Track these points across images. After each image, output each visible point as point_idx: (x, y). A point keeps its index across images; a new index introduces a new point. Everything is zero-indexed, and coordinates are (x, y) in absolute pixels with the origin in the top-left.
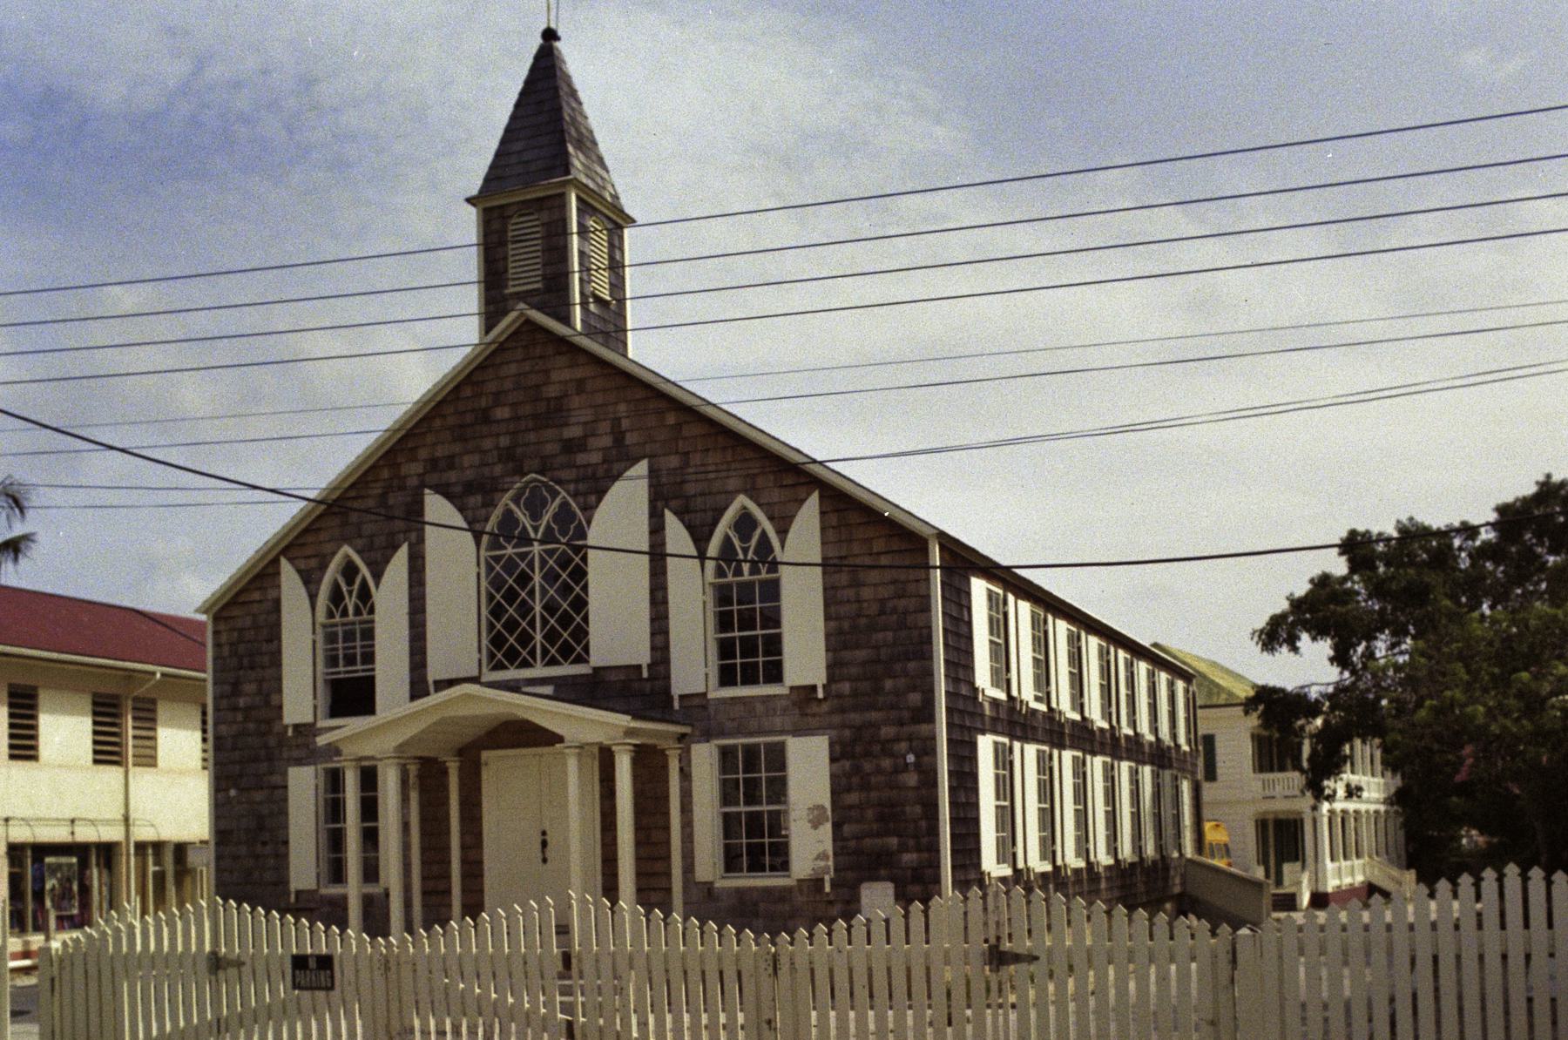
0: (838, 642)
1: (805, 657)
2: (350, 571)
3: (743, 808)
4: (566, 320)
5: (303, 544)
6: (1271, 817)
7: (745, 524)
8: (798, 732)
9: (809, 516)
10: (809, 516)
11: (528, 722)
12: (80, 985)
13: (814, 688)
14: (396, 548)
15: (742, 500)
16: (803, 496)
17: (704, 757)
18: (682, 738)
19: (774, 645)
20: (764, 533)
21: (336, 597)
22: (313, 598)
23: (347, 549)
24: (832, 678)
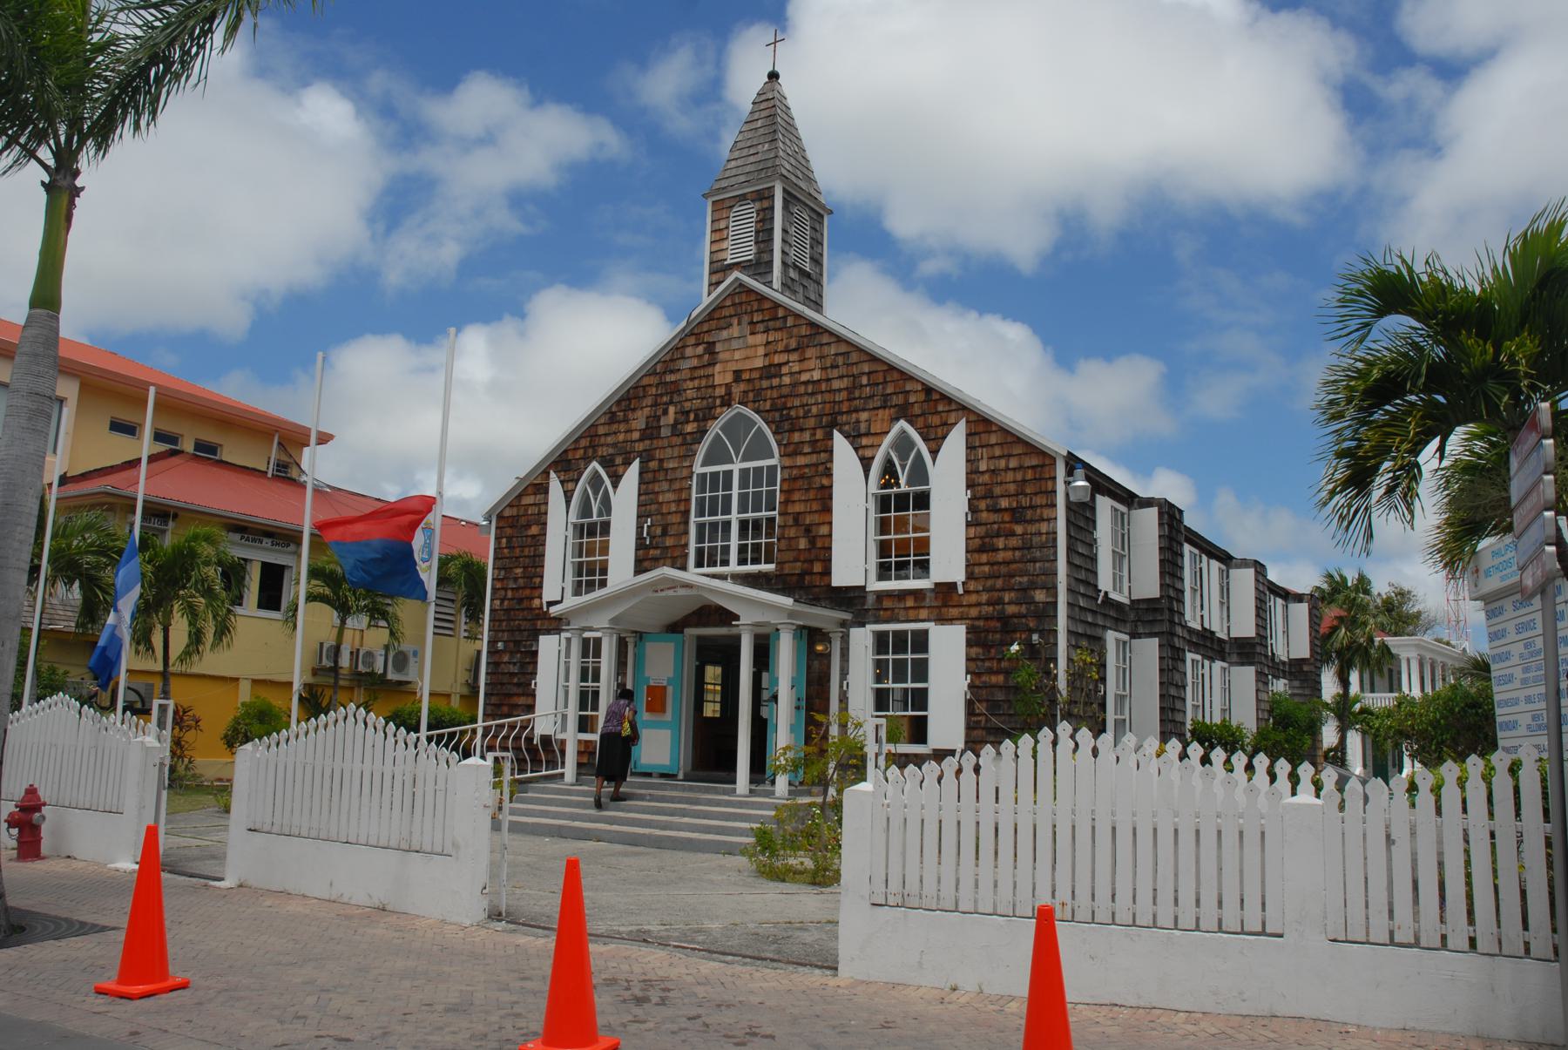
0: (978, 547)
1: (949, 559)
2: (596, 481)
3: (910, 685)
4: (769, 284)
5: (565, 461)
6: (115, 718)
7: (596, 481)
8: (942, 620)
9: (956, 442)
10: (956, 442)
11: (721, 608)
12: (430, 798)
13: (953, 585)
14: (628, 463)
15: (595, 465)
16: (951, 420)
17: (862, 639)
18: (844, 624)
19: (923, 546)
20: (919, 452)
21: (889, 469)
22: (568, 503)
23: (903, 424)
24: (970, 576)
